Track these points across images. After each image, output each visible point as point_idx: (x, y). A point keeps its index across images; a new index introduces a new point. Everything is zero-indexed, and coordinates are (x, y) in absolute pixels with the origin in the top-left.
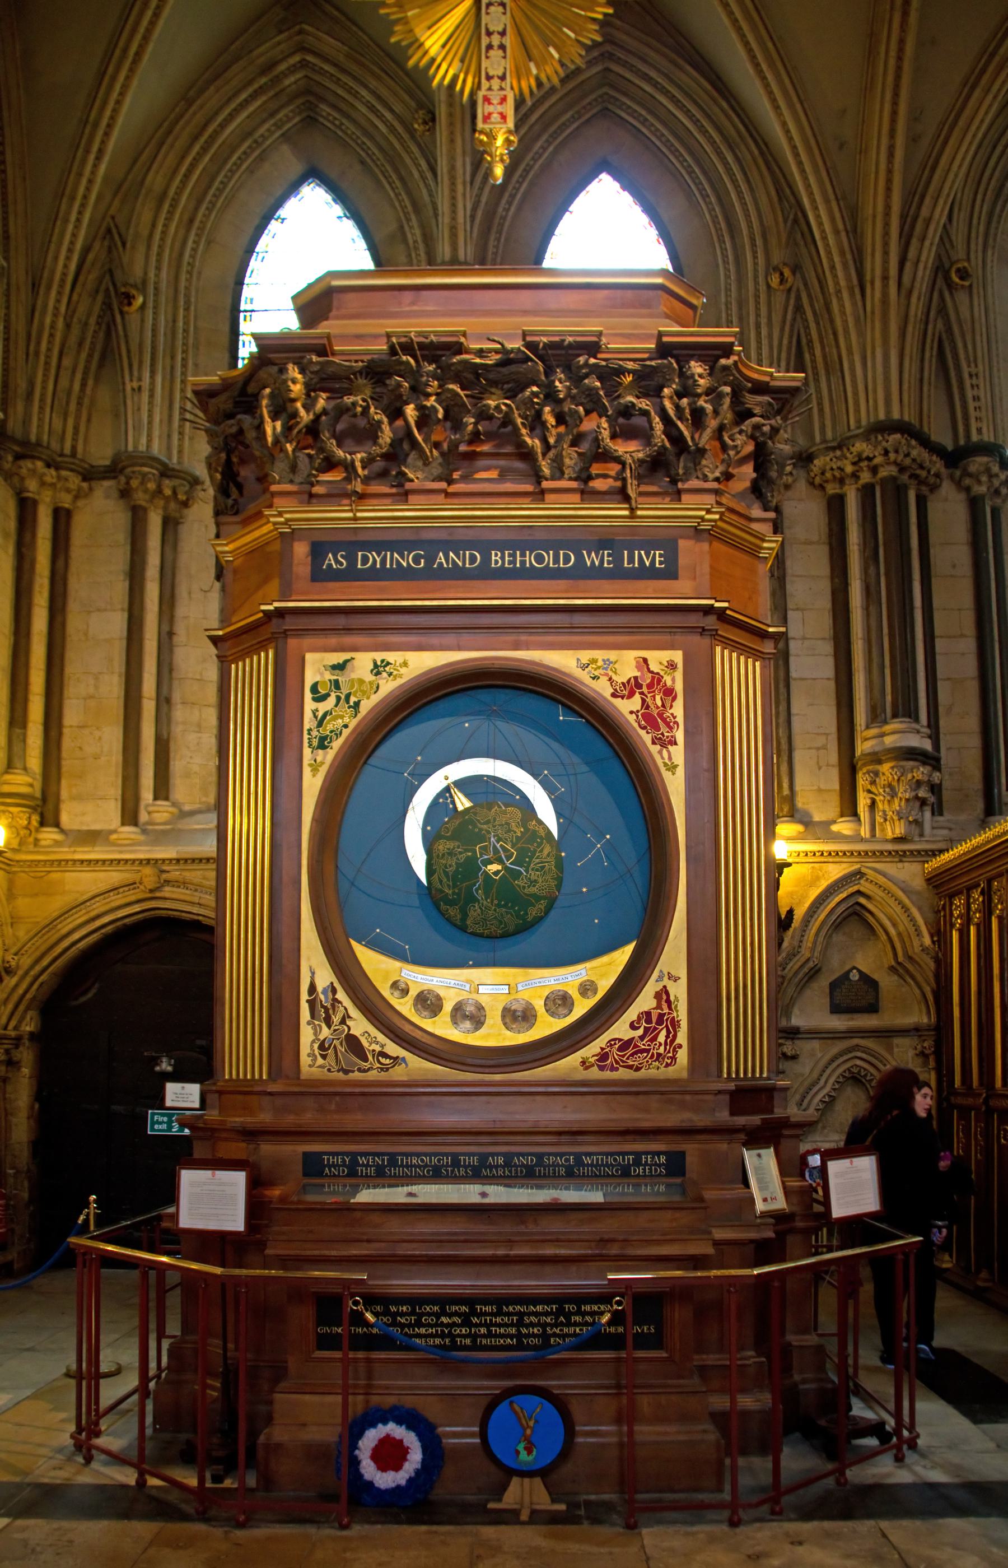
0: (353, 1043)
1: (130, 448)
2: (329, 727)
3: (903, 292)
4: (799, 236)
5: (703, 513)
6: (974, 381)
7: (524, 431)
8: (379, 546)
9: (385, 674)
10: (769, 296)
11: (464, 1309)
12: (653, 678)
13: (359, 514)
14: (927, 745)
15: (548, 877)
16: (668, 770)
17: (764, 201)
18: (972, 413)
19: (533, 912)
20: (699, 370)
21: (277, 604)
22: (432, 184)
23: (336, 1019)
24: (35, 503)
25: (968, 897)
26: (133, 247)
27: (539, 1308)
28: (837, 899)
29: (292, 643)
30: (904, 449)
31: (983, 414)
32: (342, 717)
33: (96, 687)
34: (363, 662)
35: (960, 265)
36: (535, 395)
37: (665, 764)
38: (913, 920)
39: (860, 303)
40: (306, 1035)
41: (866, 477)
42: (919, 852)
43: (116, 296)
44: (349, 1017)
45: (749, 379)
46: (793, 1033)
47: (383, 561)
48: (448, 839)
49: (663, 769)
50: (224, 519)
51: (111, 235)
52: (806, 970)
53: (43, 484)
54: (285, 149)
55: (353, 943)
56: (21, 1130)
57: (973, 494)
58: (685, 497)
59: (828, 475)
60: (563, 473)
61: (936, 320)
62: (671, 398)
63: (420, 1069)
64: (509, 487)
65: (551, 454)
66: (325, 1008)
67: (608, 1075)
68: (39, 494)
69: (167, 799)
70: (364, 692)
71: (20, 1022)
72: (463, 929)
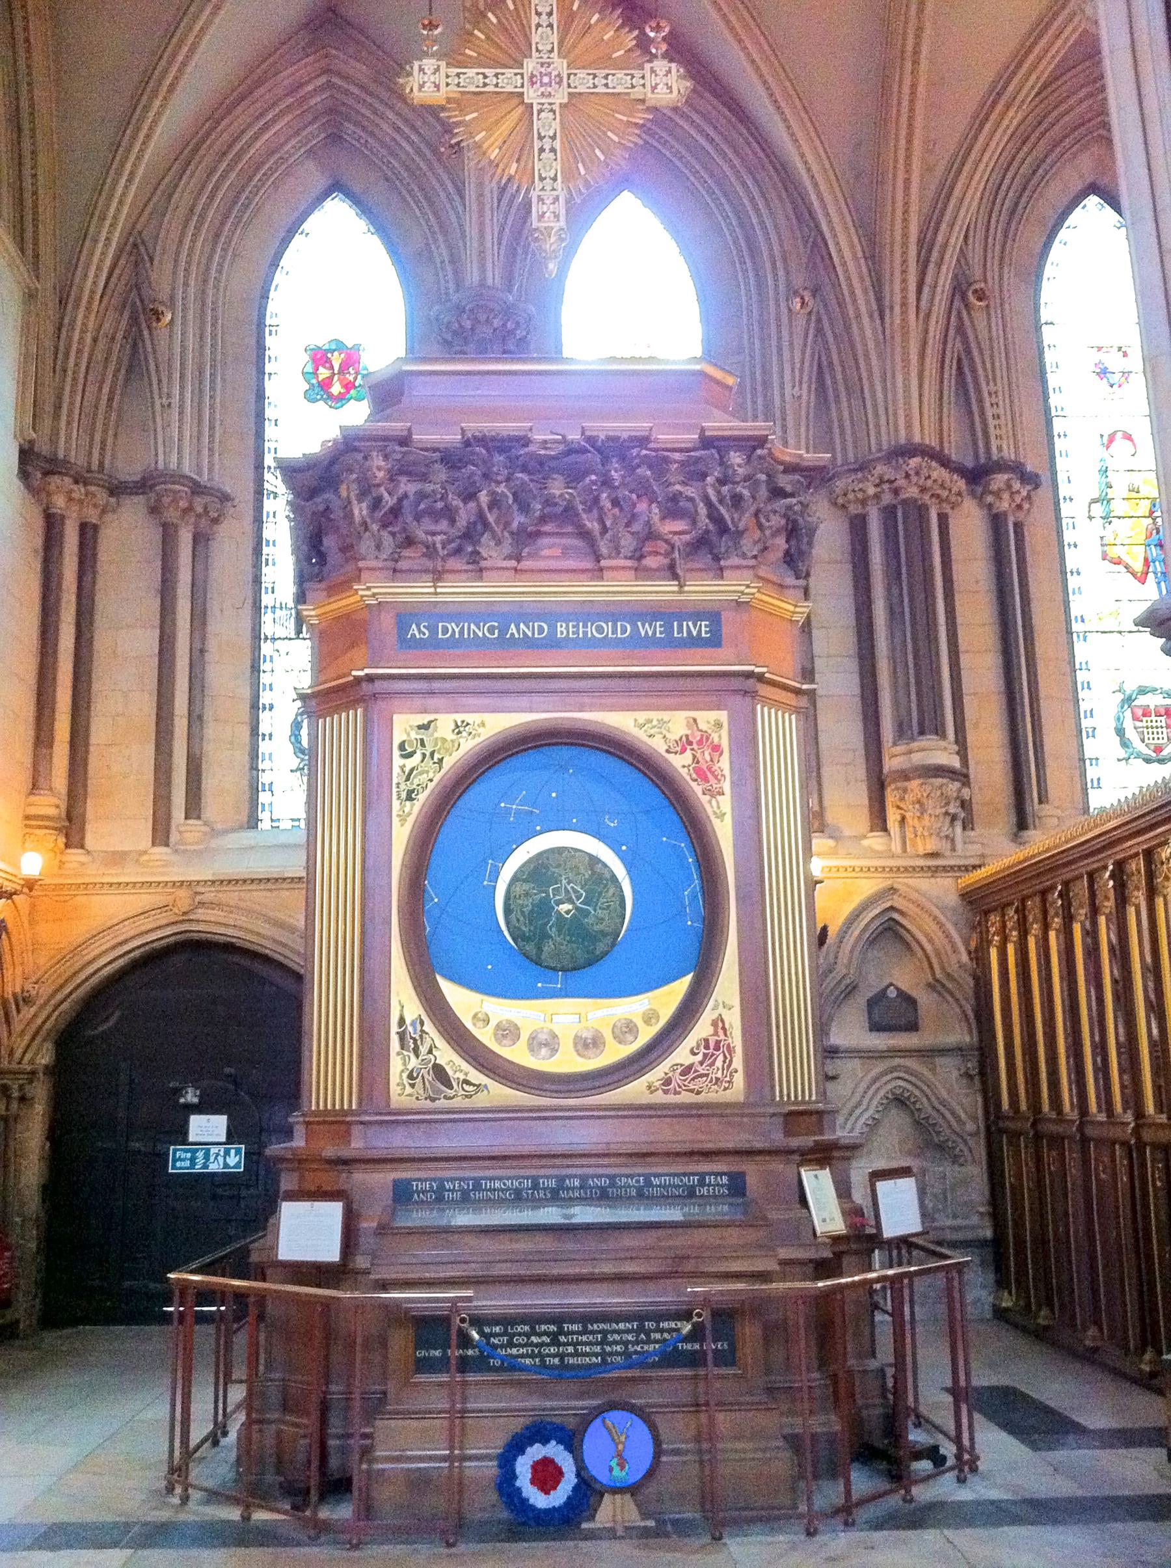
0: (440, 1073)
1: (161, 465)
3: (922, 315)
4: (818, 260)
10: (790, 319)
11: (553, 1328)
14: (956, 763)
17: (782, 221)
19: (601, 947)
20: (738, 460)
21: (367, 671)
22: (460, 209)
23: (423, 1050)
25: (1003, 916)
26: (161, 263)
27: (621, 1326)
28: (872, 915)
30: (925, 472)
31: (1002, 421)
34: (445, 723)
35: (977, 286)
36: (593, 483)
39: (880, 329)
40: (396, 1066)
41: (887, 498)
42: (952, 867)
43: (140, 313)
45: (781, 463)
46: (832, 1052)
47: (462, 632)
48: (524, 881)
49: (712, 817)
50: (306, 585)
51: (137, 251)
52: (843, 987)
54: (310, 165)
55: (438, 978)
56: (31, 1171)
57: (995, 511)
58: (726, 573)
59: (851, 496)
60: (619, 553)
62: (713, 486)
64: (571, 564)
65: (608, 536)
66: (415, 1040)
67: (671, 1099)
69: (199, 818)
70: (447, 750)
71: (36, 1054)
72: (538, 962)
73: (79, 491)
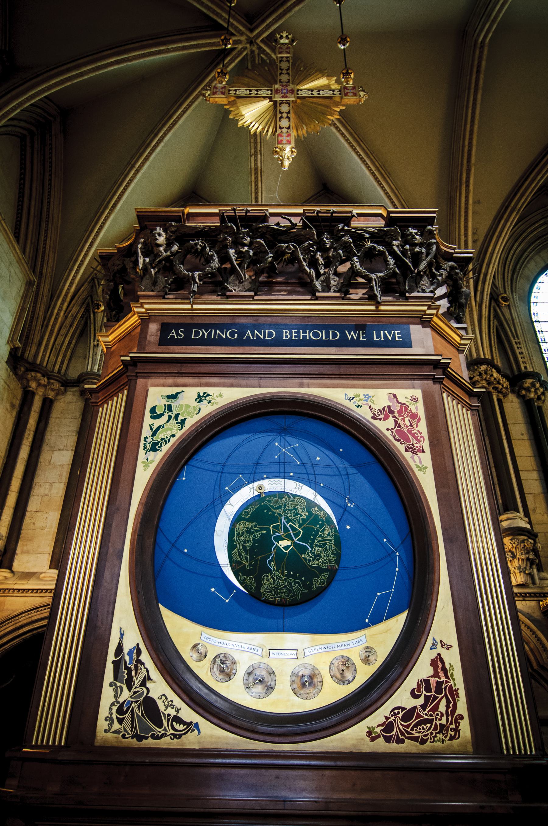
0: (150, 706)
2: (158, 438)
5: (425, 308)
6: (518, 345)
7: (304, 263)
8: (207, 326)
9: (205, 402)
12: (401, 407)
13: (195, 307)
15: (329, 553)
16: (420, 470)
18: (521, 360)
19: (317, 583)
23: (137, 681)
24: (33, 394)
29: (140, 382)
30: (489, 372)
32: (171, 429)
33: (50, 490)
34: (190, 394)
36: (312, 246)
37: (418, 466)
38: (539, 639)
40: (107, 696)
44: (150, 679)
47: (209, 335)
48: (247, 520)
53: (39, 385)
61: (494, 320)
63: (211, 736)
65: (322, 278)
66: (129, 670)
67: (394, 747)
68: (36, 390)
70: (189, 413)
73: (44, 381)
